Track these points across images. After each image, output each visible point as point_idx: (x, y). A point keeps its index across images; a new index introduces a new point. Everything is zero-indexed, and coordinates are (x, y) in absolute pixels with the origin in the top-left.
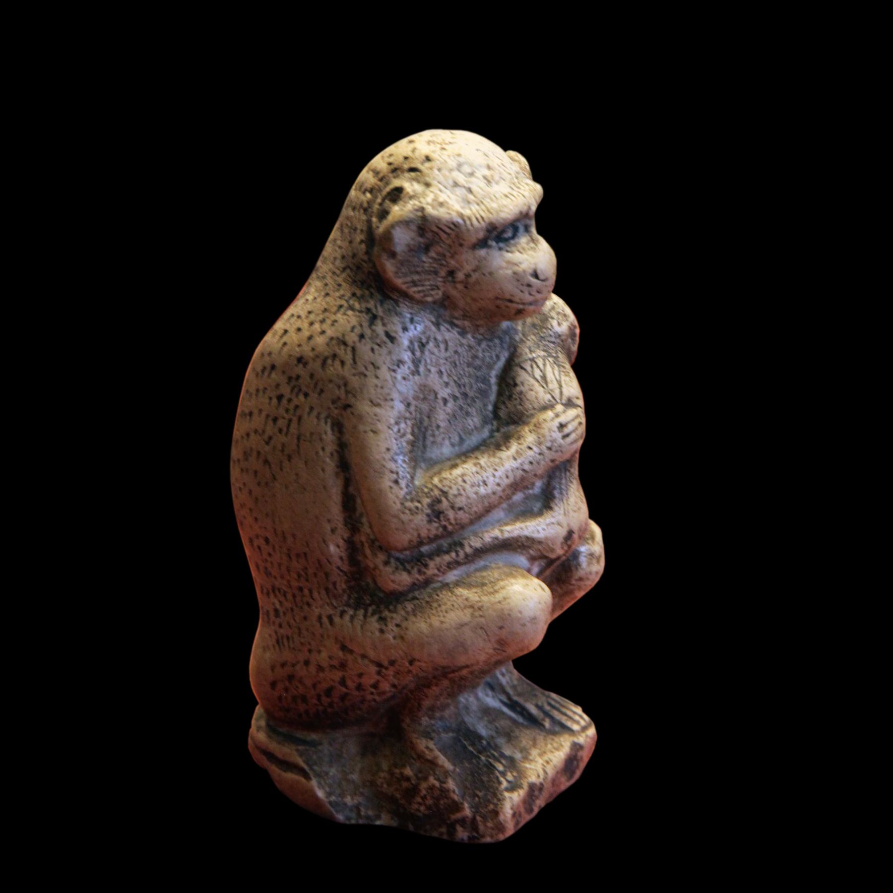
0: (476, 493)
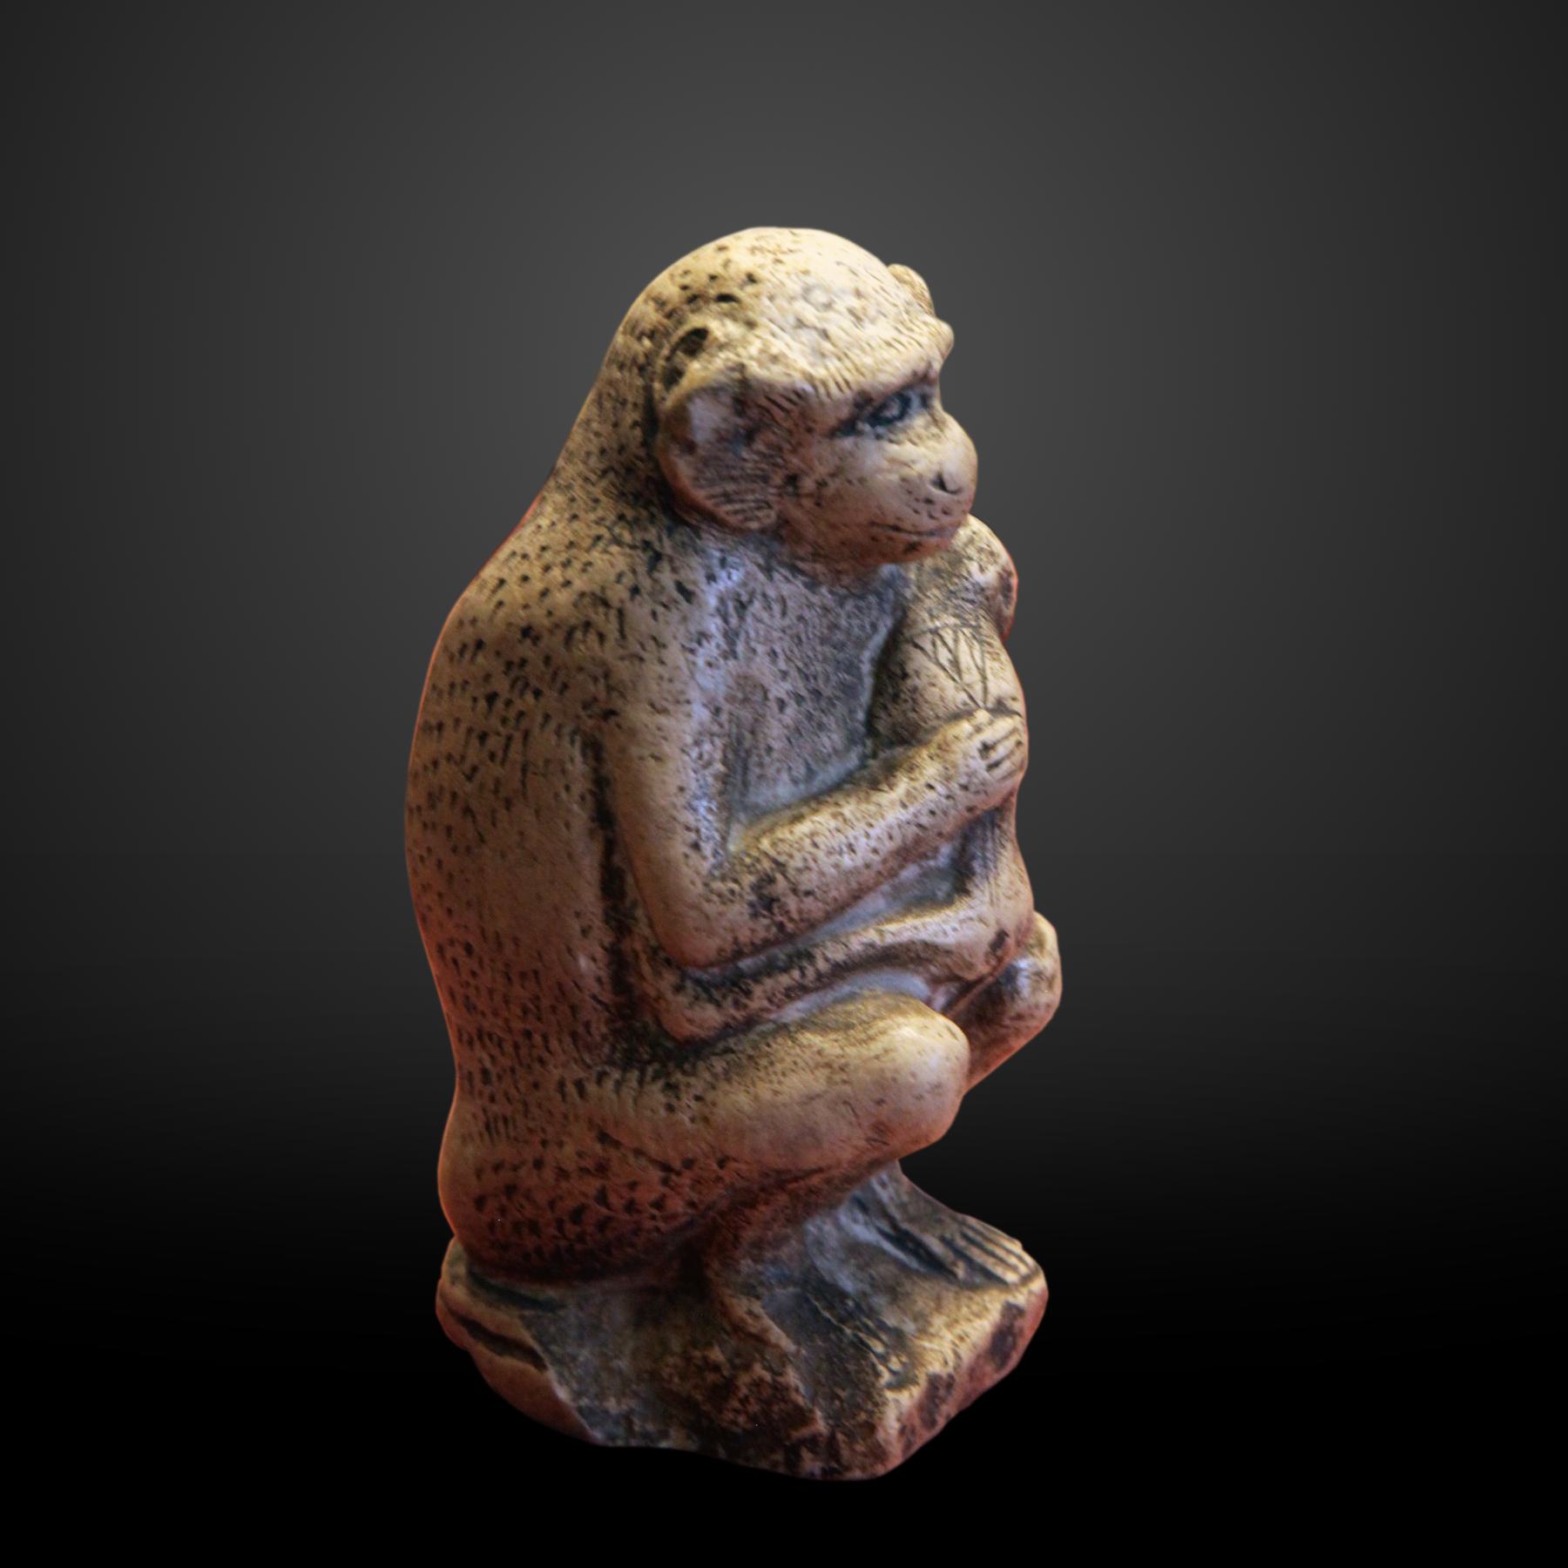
0: (836, 866)
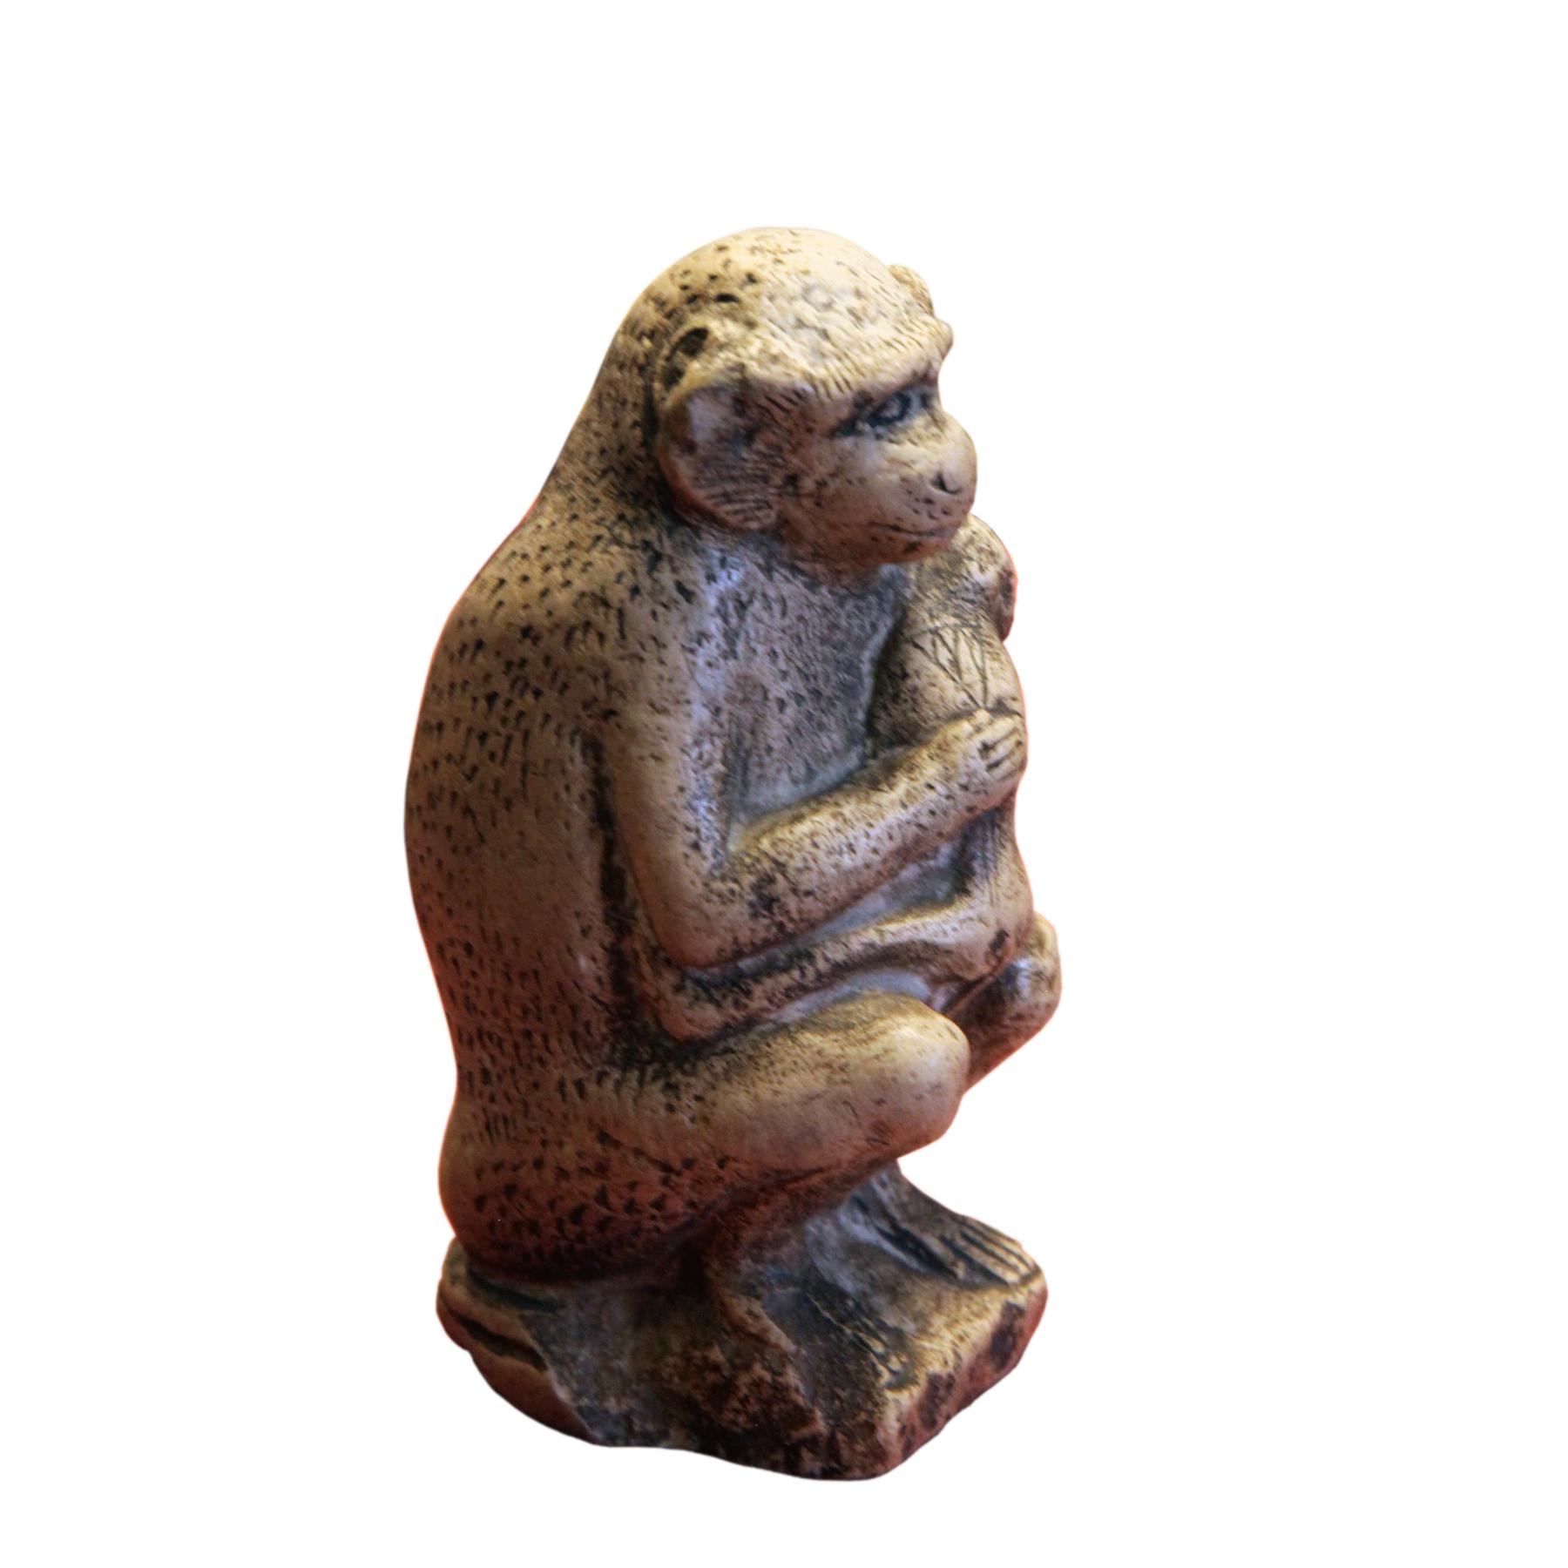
0: (836, 866)
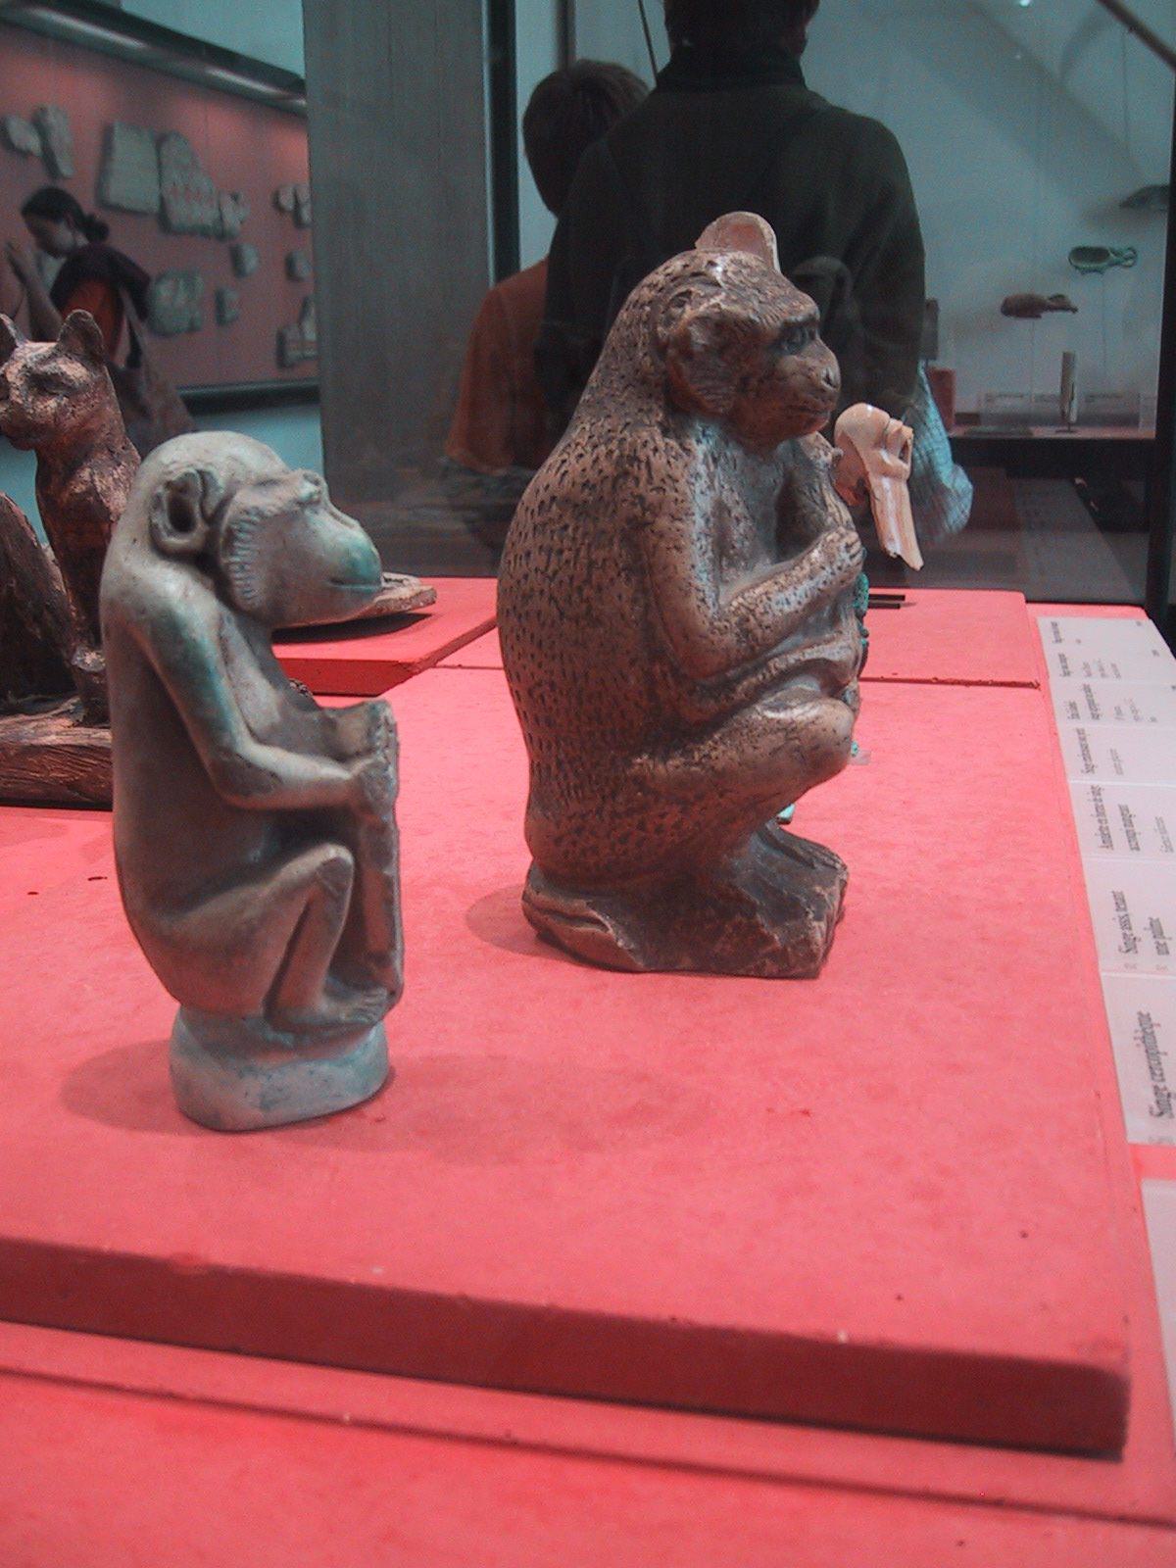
0: (781, 611)
